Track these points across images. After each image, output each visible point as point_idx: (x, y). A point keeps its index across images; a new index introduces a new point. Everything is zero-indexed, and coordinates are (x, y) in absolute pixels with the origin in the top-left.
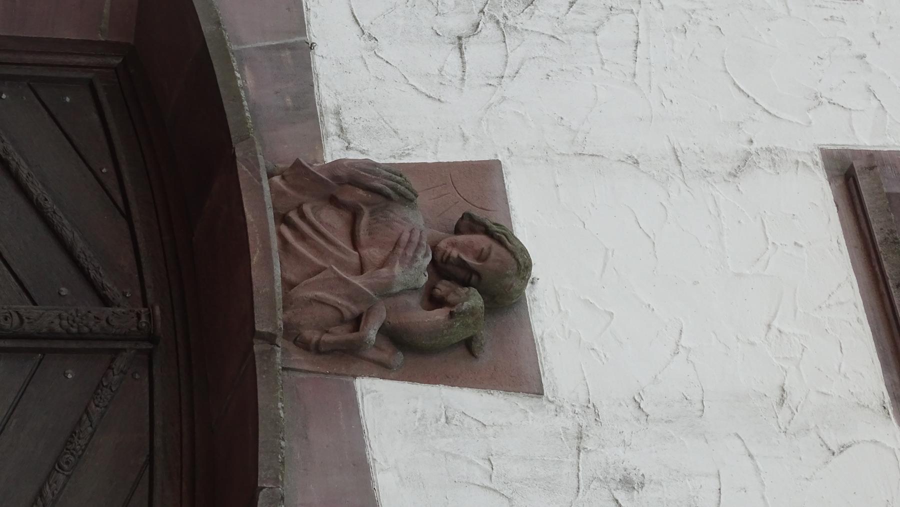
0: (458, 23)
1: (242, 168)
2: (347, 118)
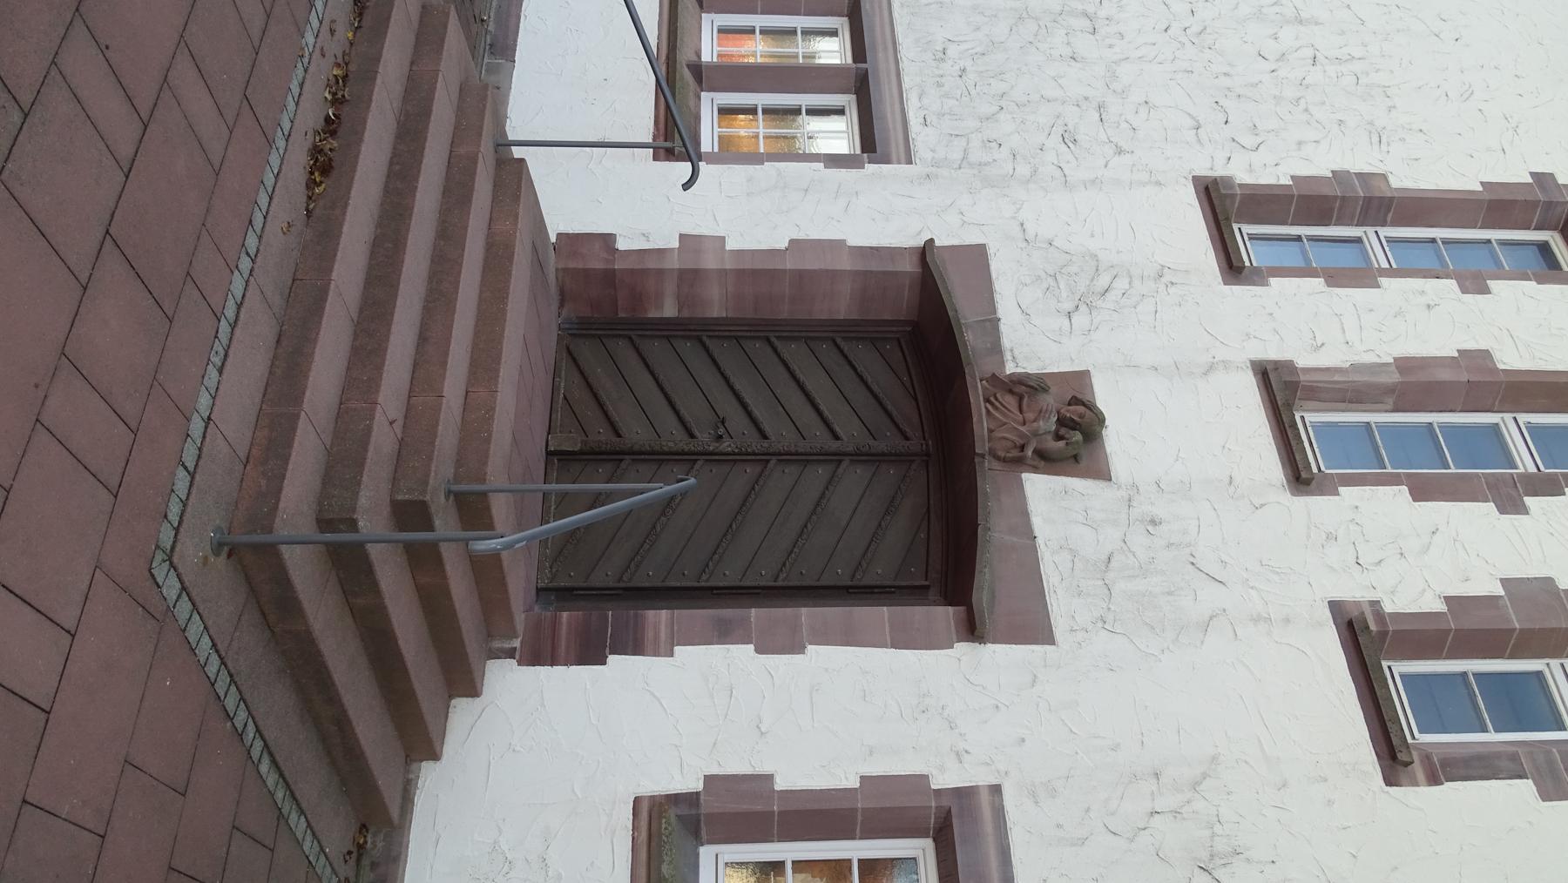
0: (1068, 306)
2: (1016, 352)
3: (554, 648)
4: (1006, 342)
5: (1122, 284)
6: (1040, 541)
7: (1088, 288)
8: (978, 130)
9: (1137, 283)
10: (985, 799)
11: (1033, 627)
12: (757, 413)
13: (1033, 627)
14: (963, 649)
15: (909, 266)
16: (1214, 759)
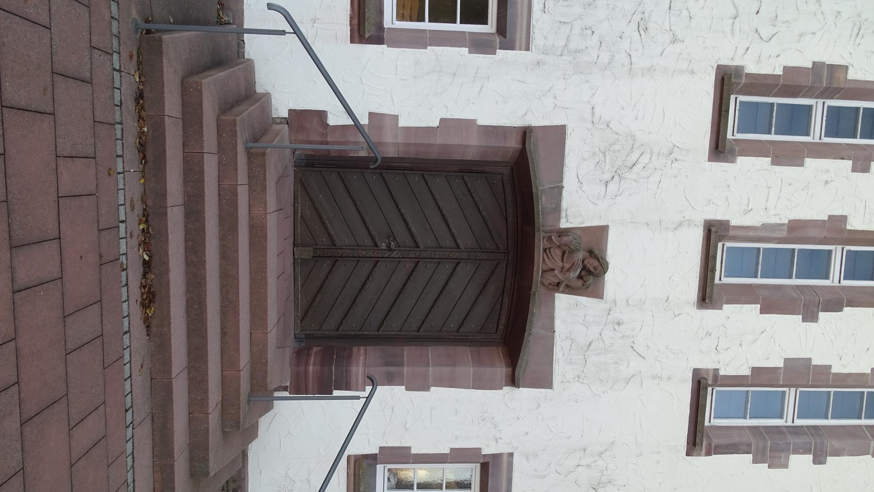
0: (607, 176)
1: (536, 240)
2: (569, 211)
3: (306, 386)
4: (564, 204)
5: (644, 160)
6: (557, 334)
7: (623, 162)
8: (580, 17)
9: (654, 158)
10: (505, 458)
11: (544, 381)
12: (413, 229)
13: (544, 381)
14: (507, 389)
15: (514, 144)
16: (613, 443)
